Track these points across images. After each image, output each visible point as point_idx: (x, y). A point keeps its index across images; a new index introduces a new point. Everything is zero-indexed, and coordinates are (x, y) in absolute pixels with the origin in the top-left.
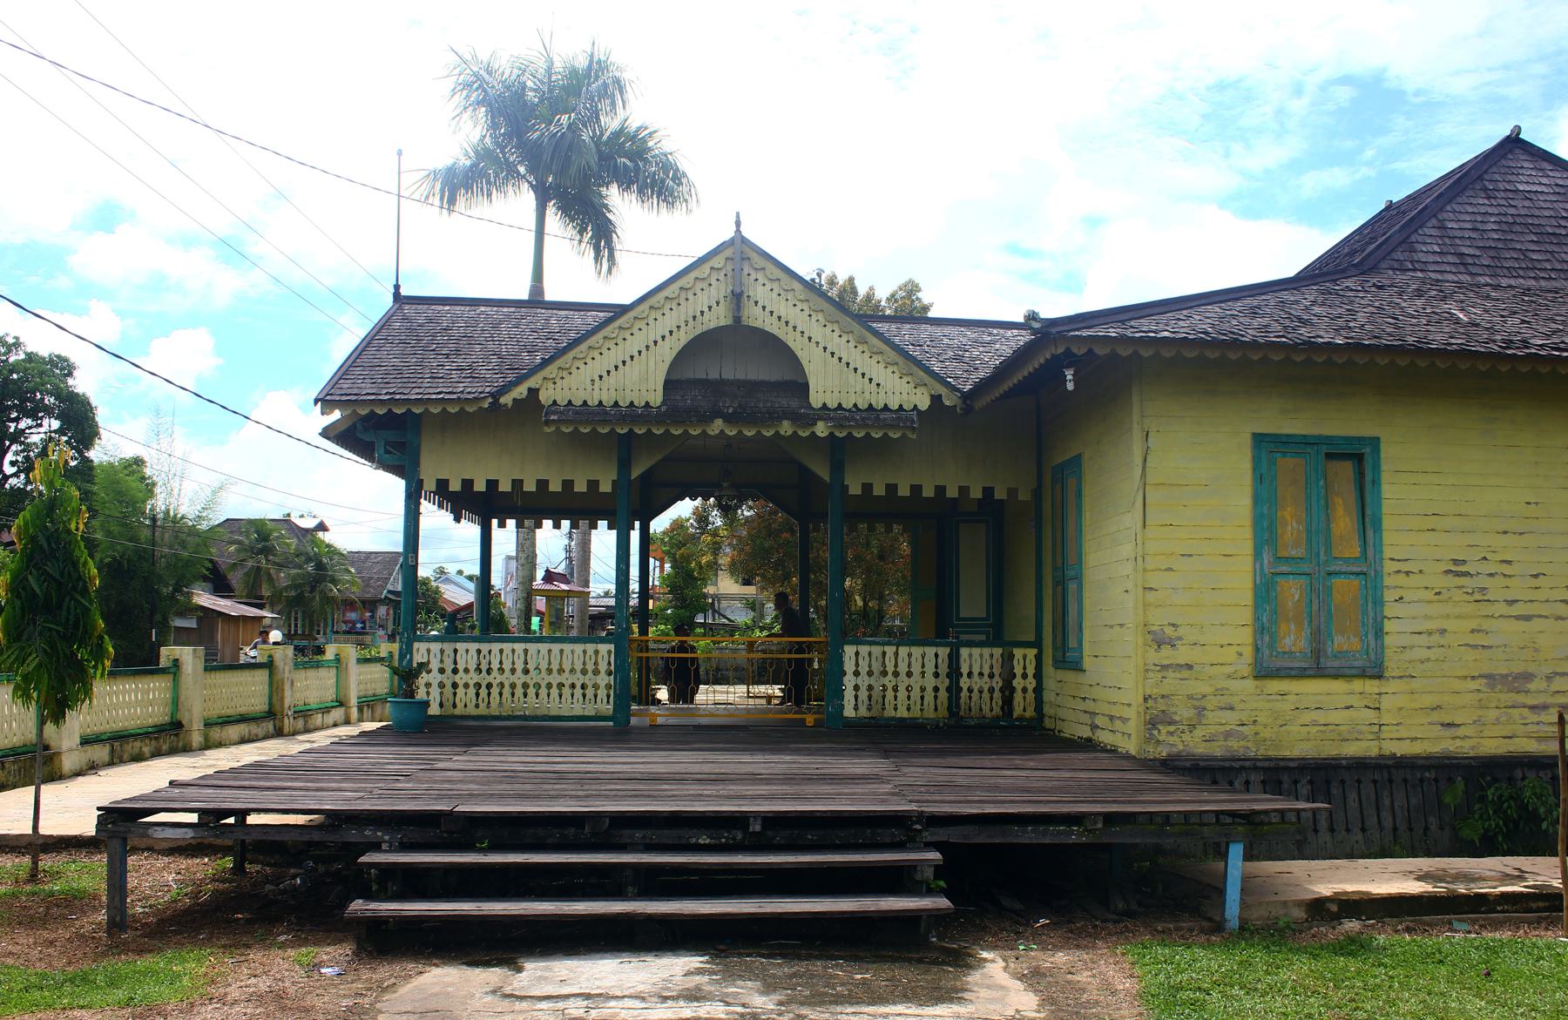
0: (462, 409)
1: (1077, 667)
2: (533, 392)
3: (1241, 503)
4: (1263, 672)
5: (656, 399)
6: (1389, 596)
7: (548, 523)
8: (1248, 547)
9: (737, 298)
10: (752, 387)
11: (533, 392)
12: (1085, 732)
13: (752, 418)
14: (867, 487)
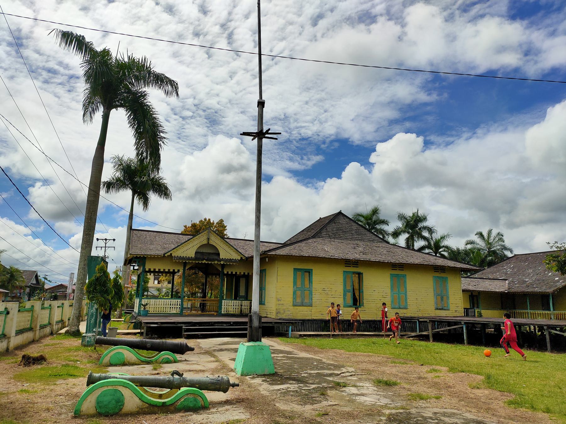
1: (264, 304)
2: (171, 254)
3: (291, 279)
4: (294, 305)
5: (193, 256)
6: (313, 294)
8: (292, 286)
9: (208, 239)
10: (209, 254)
11: (171, 254)
12: (265, 315)
13: (210, 260)
14: (228, 272)
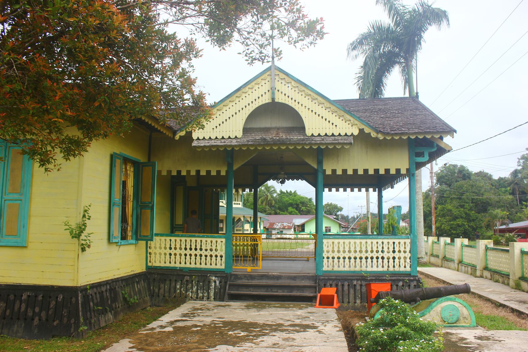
0: (393, 138)
7: (326, 190)
9: (273, 90)
